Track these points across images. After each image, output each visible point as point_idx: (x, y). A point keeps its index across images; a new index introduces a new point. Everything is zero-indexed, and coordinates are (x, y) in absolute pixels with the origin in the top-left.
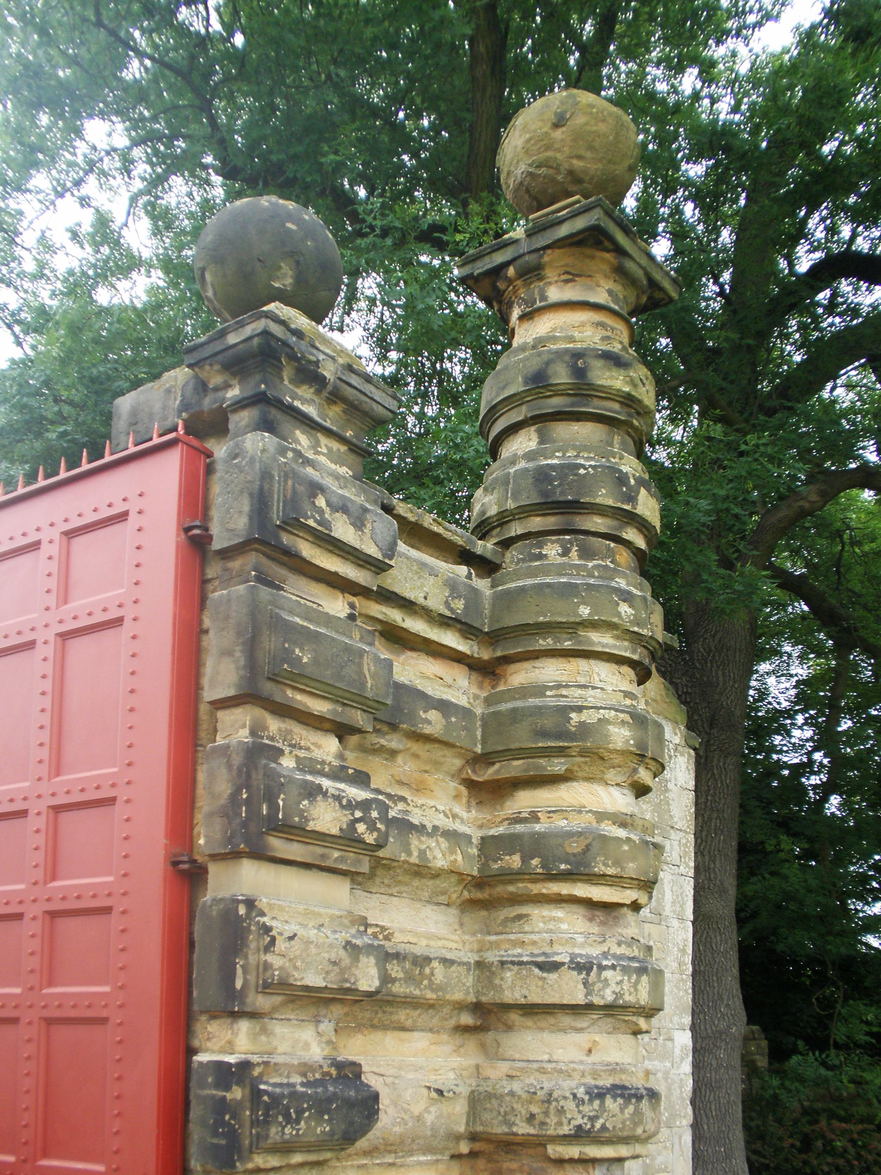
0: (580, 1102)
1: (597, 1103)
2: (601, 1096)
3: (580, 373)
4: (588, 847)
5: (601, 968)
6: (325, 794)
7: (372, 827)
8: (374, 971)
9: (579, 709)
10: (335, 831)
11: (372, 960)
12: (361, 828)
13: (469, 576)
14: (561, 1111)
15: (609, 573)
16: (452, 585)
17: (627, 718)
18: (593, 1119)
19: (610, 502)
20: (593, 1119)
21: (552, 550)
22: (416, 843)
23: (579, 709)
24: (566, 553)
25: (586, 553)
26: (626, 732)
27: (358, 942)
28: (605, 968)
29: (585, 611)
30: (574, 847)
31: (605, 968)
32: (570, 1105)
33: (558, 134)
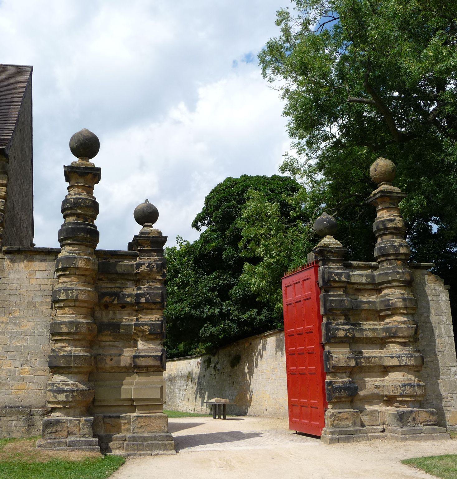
0: (400, 387)
1: (404, 387)
2: (405, 386)
3: (384, 225)
4: (396, 330)
5: (402, 357)
6: (340, 329)
7: (350, 333)
8: (354, 362)
9: (391, 300)
10: (343, 336)
11: (353, 360)
12: (348, 334)
13: (372, 272)
14: (397, 390)
15: (395, 268)
16: (367, 276)
17: (401, 300)
18: (404, 391)
19: (393, 252)
20: (404, 391)
21: (385, 264)
22: (365, 333)
23: (391, 300)
24: (387, 265)
25: (391, 264)
26: (401, 304)
27: (350, 357)
28: (402, 357)
29: (390, 278)
30: (393, 330)
31: (402, 357)
32: (399, 388)
33: (376, 173)
